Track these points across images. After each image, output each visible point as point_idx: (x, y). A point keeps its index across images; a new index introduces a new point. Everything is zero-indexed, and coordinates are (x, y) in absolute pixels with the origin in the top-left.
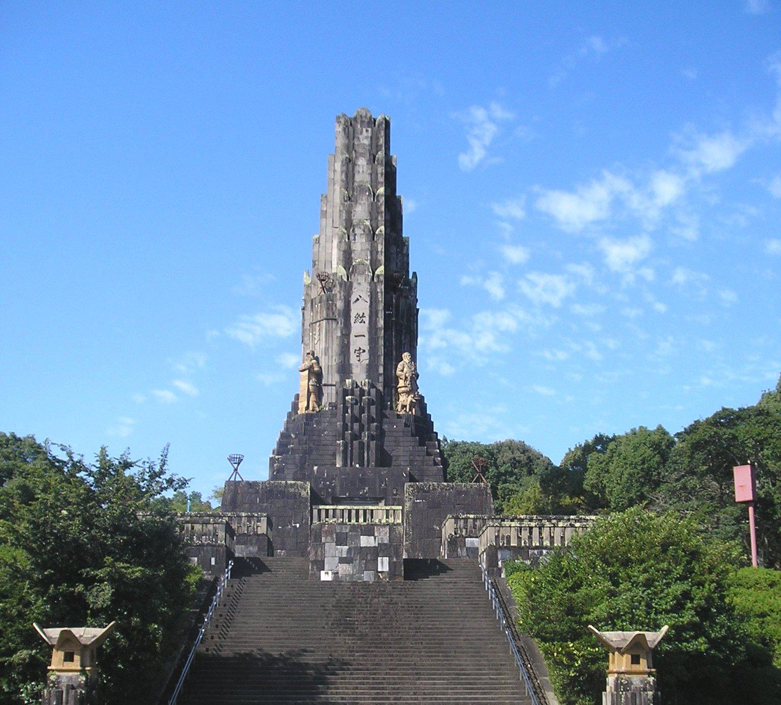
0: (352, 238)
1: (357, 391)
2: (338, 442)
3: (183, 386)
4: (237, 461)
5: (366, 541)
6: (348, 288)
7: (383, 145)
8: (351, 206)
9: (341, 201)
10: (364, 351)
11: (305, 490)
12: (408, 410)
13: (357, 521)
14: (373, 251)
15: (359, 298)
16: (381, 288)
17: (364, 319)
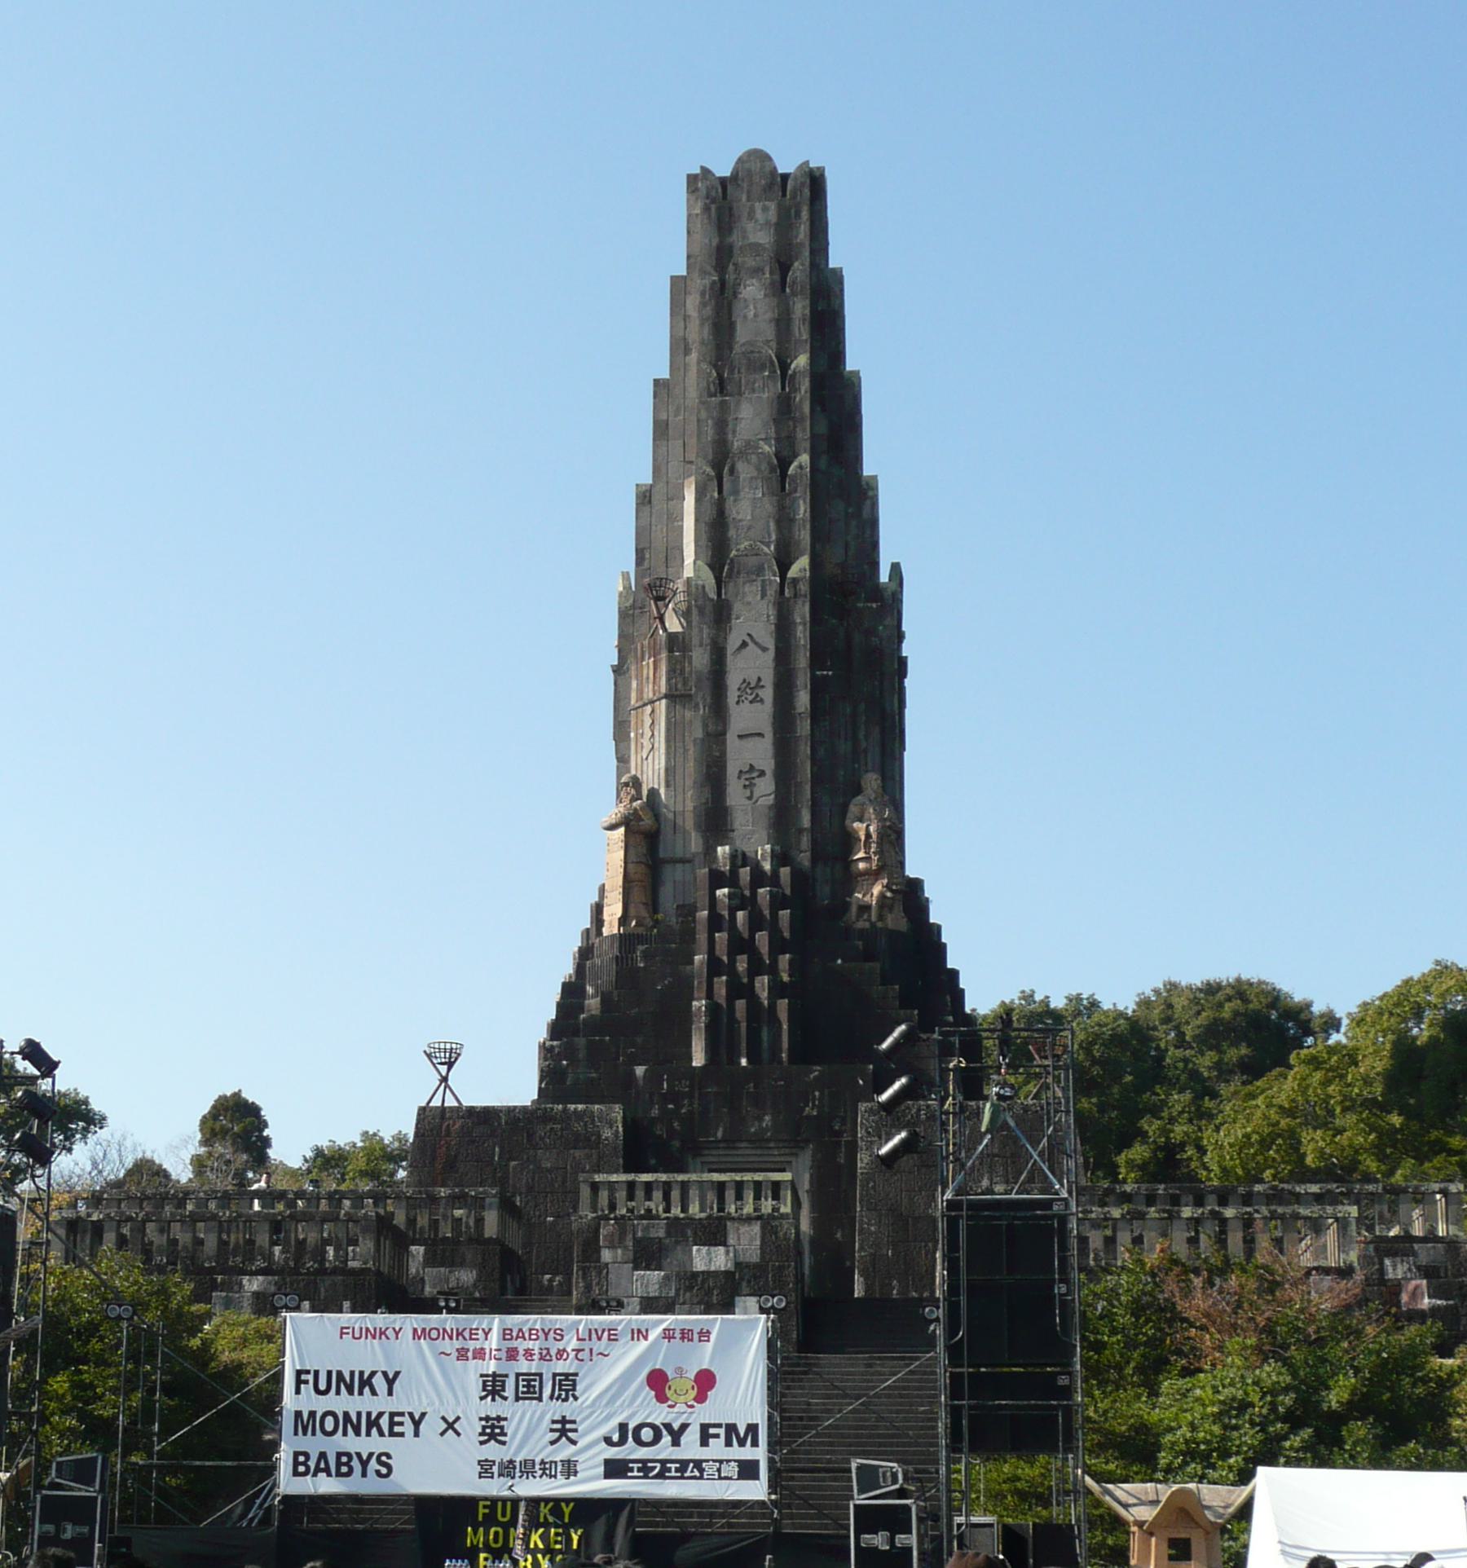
0: (726, 486)
1: (745, 873)
4: (447, 1058)
5: (709, 1259)
7: (807, 243)
8: (724, 407)
9: (701, 396)
10: (762, 773)
12: (874, 919)
13: (684, 1209)
14: (784, 519)
15: (748, 640)
16: (802, 612)
17: (761, 692)
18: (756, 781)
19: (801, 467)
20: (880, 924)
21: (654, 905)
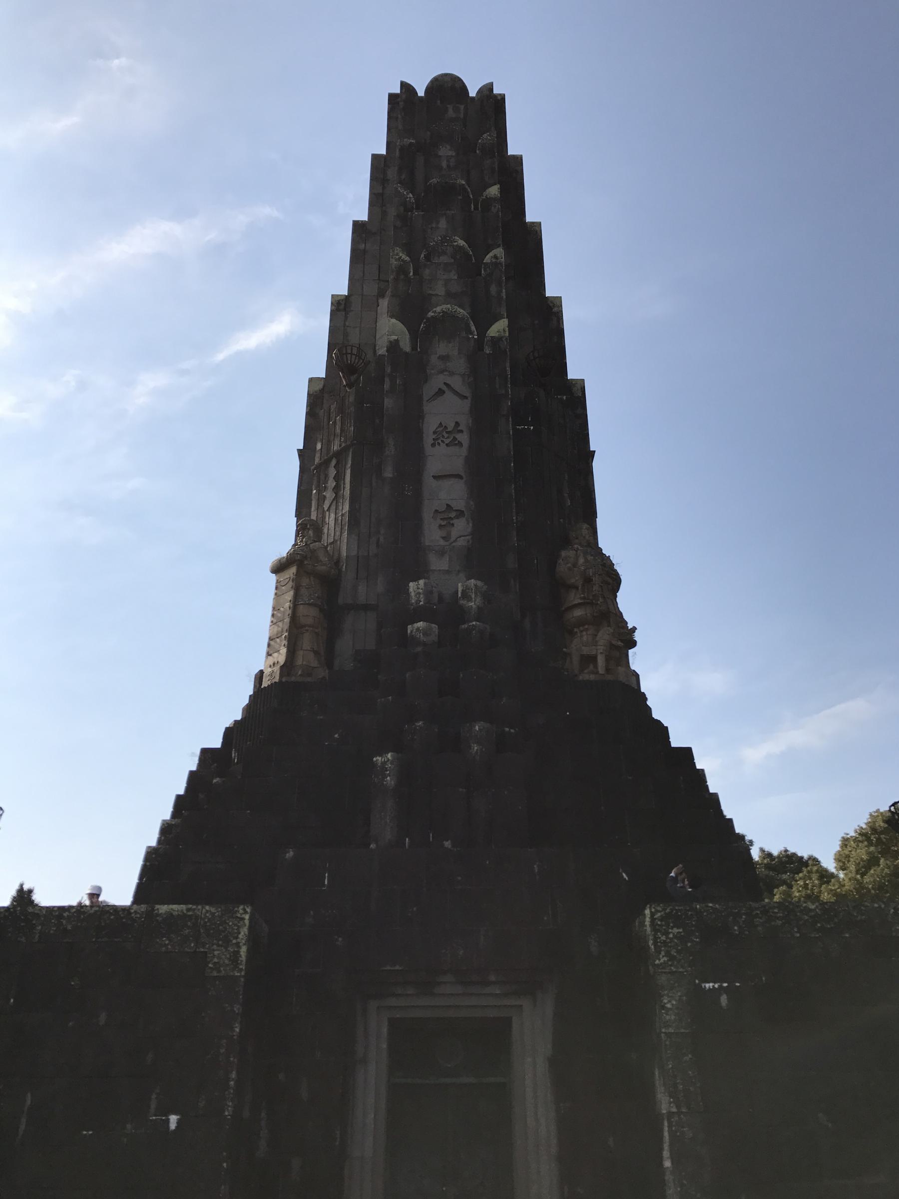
2: (378, 759)
12: (601, 670)
15: (445, 388)
17: (459, 437)
18: (455, 521)
19: (495, 257)
20: (610, 677)
21: (328, 655)
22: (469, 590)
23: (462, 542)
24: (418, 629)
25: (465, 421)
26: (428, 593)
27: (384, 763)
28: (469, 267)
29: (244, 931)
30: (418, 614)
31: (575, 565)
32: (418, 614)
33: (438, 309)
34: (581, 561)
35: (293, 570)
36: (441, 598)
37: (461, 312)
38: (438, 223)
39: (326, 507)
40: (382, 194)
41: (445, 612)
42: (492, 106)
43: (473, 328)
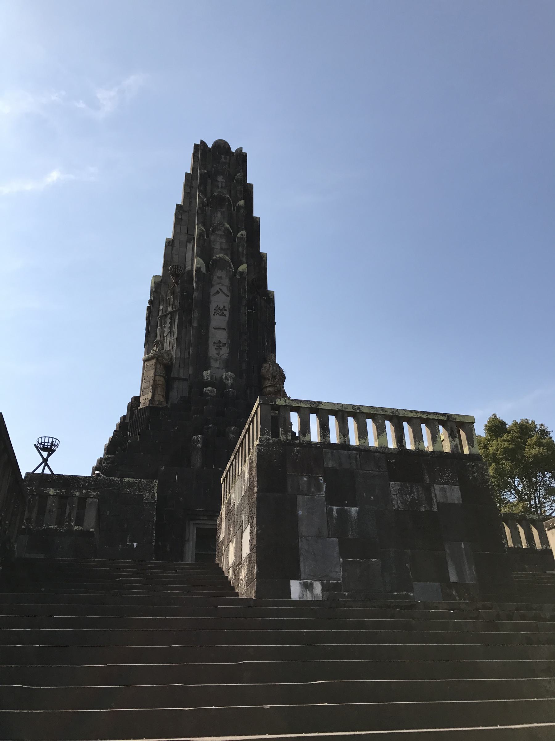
3: (77, 494)
6: (206, 280)
11: (150, 492)
15: (219, 291)
17: (225, 312)
18: (222, 348)
19: (242, 235)
21: (167, 397)
22: (228, 377)
23: (225, 356)
24: (208, 390)
25: (228, 306)
26: (212, 376)
27: (198, 439)
28: (230, 237)
29: (156, 488)
30: (207, 384)
31: (269, 370)
32: (207, 384)
33: (218, 256)
34: (271, 369)
35: (154, 361)
36: (216, 379)
37: (228, 258)
38: (217, 214)
39: (165, 335)
40: (190, 193)
41: (219, 384)
42: (241, 158)
43: (232, 266)
